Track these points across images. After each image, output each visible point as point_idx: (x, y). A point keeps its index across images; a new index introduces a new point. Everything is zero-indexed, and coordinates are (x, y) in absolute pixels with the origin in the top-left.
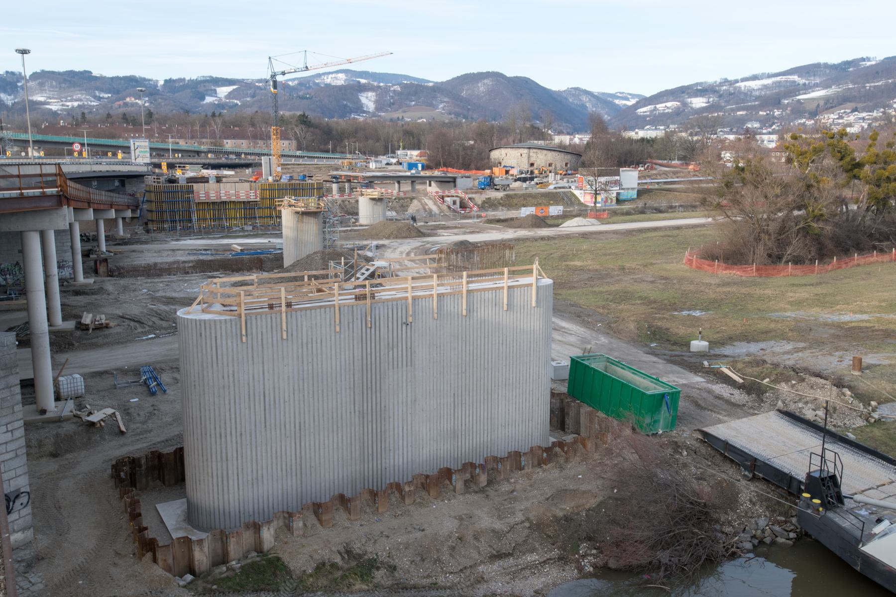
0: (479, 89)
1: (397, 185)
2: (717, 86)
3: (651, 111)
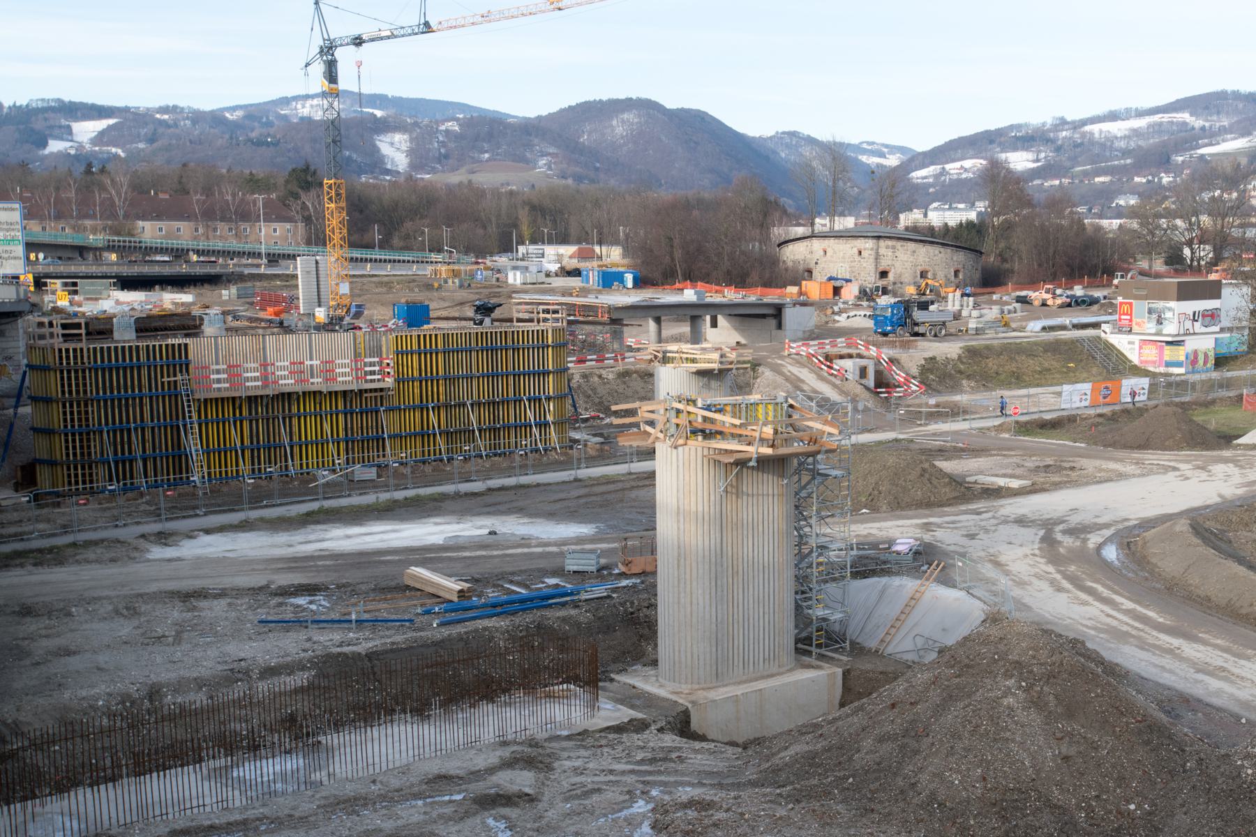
0: (613, 131)
1: (652, 325)
2: (1050, 131)
3: (937, 176)
